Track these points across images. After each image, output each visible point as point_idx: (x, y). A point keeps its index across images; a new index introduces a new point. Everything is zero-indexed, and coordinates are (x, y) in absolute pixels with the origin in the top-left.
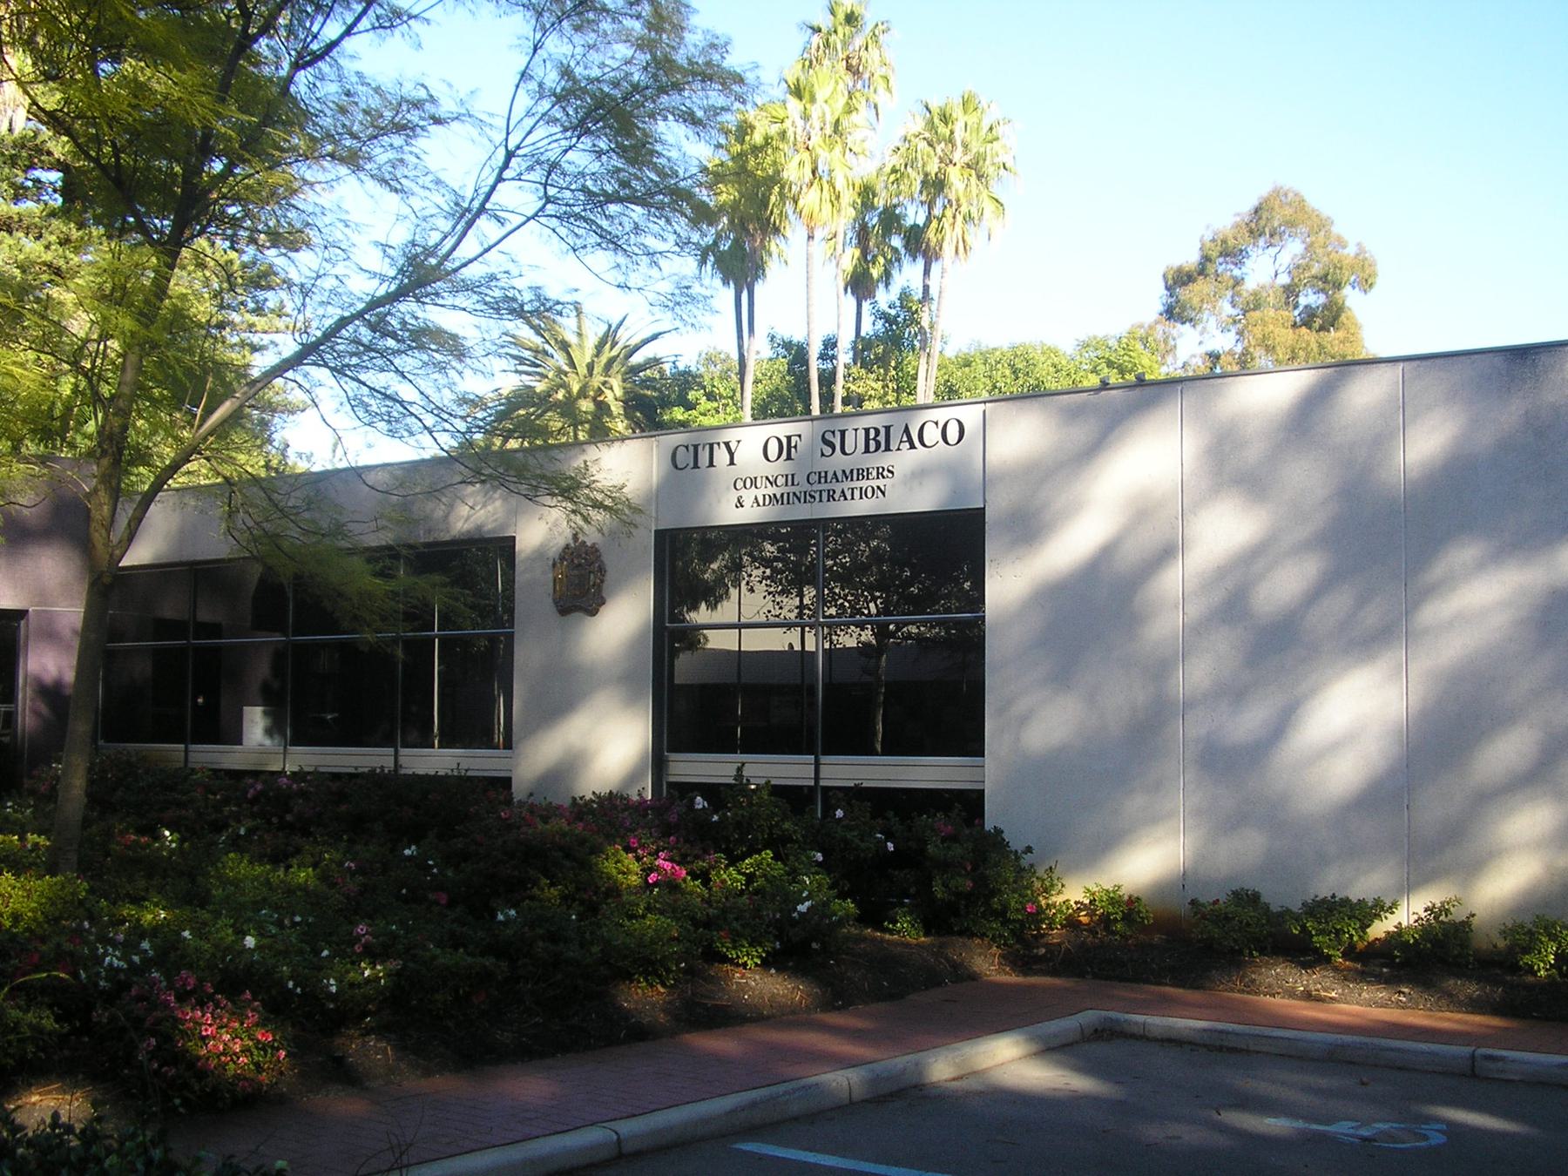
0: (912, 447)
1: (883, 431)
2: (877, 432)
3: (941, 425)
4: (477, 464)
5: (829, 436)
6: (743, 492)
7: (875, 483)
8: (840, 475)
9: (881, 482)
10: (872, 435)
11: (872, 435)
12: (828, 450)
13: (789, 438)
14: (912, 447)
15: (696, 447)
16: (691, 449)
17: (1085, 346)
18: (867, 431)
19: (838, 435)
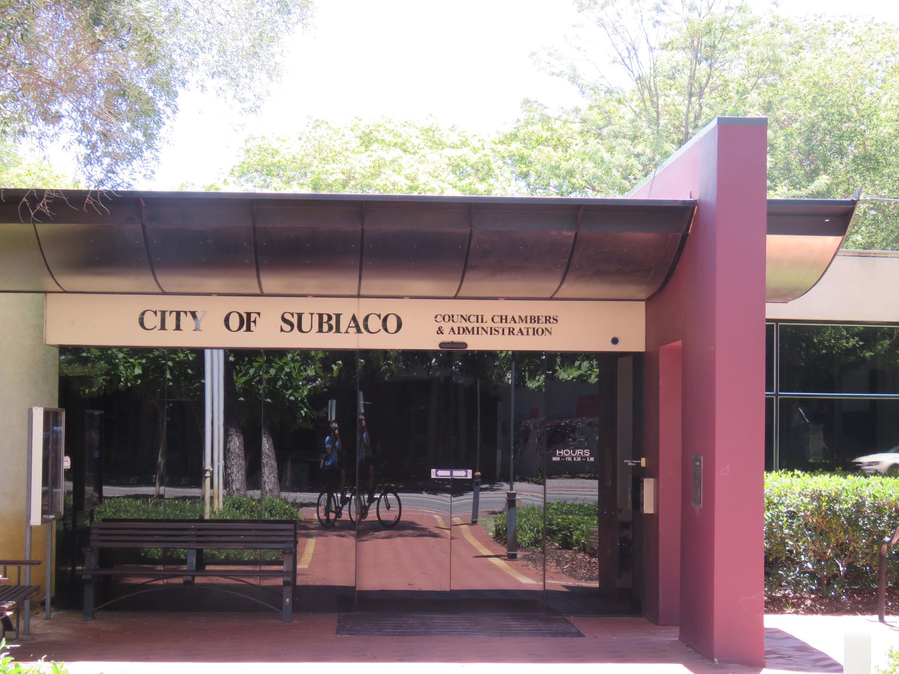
0: (359, 331)
1: (334, 317)
2: (330, 318)
3: (382, 318)
4: (772, 145)
5: (288, 317)
6: (442, 324)
7: (544, 326)
8: (517, 319)
9: (548, 326)
10: (325, 318)
11: (325, 318)
12: (287, 327)
13: (249, 315)
14: (359, 331)
15: (163, 313)
16: (159, 314)
17: (579, 634)
18: (321, 316)
19: (296, 316)
